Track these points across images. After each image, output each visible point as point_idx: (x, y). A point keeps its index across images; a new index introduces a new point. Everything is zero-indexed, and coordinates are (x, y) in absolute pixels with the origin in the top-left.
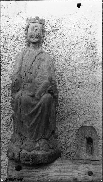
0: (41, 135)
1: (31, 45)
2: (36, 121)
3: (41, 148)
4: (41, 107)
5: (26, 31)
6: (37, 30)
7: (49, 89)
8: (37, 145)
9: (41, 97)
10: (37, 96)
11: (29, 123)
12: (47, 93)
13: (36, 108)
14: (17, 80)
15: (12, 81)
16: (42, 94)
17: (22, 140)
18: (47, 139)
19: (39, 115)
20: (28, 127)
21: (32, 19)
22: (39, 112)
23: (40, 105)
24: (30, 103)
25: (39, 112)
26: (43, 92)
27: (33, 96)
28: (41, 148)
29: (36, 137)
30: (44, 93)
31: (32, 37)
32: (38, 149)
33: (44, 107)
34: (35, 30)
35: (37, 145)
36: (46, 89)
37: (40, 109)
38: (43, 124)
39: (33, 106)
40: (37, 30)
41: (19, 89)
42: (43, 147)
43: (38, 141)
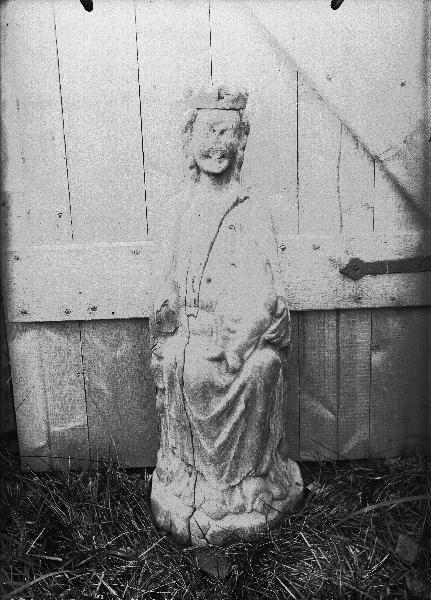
0: (247, 468)
1: (205, 178)
2: (233, 432)
3: (249, 508)
4: (249, 386)
5: (186, 135)
6: (222, 132)
7: (267, 335)
8: (237, 499)
9: (242, 361)
10: (232, 360)
11: (214, 439)
12: (261, 349)
13: (230, 395)
14: (165, 304)
15: (89, 392)
16: (247, 354)
17: (193, 477)
18: (265, 476)
19: (241, 416)
20: (210, 451)
21: (203, 96)
22: (241, 407)
23: (243, 387)
24: (212, 386)
25: (241, 407)
26: (250, 346)
27: (221, 359)
28: (249, 508)
29: (232, 476)
30: (255, 348)
31: (207, 156)
32: (241, 510)
33: (253, 392)
34: (217, 133)
35: (237, 499)
36: (259, 338)
37: (242, 398)
38: (251, 440)
39: (223, 391)
40: (222, 132)
41: (177, 329)
42: (253, 503)
43: (240, 484)
